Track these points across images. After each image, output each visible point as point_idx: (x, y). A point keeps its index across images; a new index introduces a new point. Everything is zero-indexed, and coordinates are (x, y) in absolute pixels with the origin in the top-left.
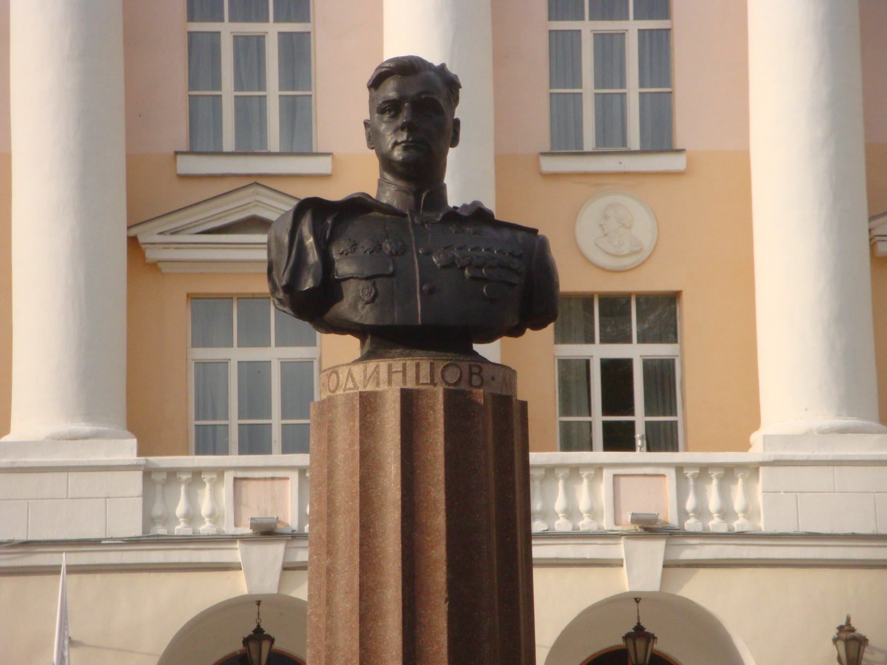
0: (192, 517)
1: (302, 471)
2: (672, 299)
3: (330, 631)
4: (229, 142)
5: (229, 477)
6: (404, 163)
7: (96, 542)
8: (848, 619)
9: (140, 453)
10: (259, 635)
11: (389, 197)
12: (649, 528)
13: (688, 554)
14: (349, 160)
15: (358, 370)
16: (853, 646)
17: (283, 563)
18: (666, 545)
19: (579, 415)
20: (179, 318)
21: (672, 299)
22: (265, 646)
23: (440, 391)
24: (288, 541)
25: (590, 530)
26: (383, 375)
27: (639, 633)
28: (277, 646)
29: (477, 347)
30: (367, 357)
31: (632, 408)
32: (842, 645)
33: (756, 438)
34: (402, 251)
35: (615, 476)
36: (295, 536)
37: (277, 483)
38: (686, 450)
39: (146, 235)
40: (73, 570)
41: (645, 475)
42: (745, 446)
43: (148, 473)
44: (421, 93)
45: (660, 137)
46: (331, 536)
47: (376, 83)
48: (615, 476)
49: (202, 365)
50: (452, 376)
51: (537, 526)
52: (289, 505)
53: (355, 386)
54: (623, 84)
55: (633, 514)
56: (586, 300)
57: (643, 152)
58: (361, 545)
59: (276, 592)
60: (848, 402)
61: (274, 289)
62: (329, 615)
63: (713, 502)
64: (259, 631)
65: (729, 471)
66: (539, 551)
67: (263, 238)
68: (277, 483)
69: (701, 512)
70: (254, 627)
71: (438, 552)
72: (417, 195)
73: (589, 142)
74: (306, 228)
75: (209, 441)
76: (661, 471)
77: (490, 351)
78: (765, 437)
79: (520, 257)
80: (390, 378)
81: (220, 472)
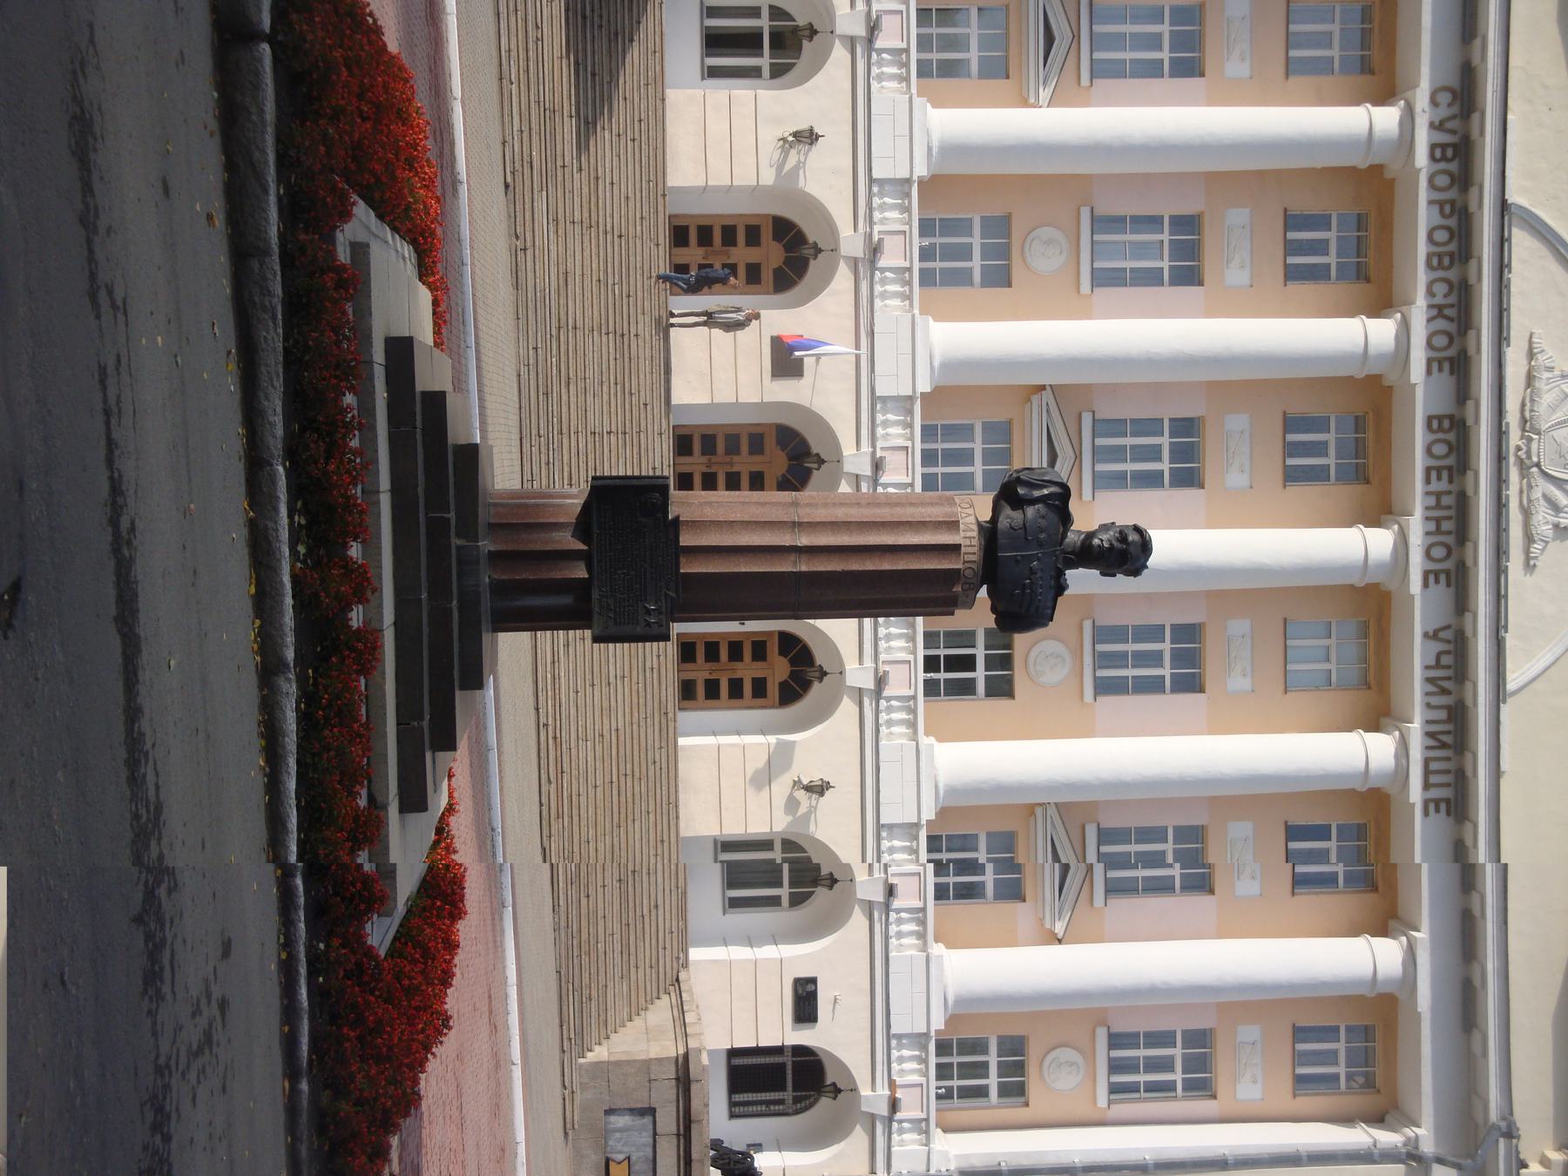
0: (886, 424)
1: (912, 485)
3: (826, 505)
4: (1100, 441)
5: (909, 444)
6: (1091, 545)
10: (821, 462)
11: (1072, 537)
12: (881, 681)
13: (866, 701)
14: (1094, 513)
15: (972, 519)
20: (999, 416)
25: (872, 651)
27: (823, 674)
30: (979, 525)
31: (949, 673)
33: (932, 740)
34: (1040, 545)
36: (875, 481)
39: (1047, 396)
40: (858, 357)
41: (501, 789)
42: (927, 734)
43: (911, 399)
45: (1105, 687)
46: (878, 505)
47: (1137, 529)
49: (971, 428)
51: (881, 620)
56: (1009, 646)
57: (1095, 678)
60: (952, 791)
61: (1018, 471)
64: (823, 462)
65: (913, 725)
66: (867, 622)
67: (1045, 465)
69: (890, 709)
71: (886, 565)
72: (1072, 553)
73: (1100, 648)
74: (1053, 489)
75: (928, 432)
77: (983, 592)
80: (968, 538)
81: (912, 438)
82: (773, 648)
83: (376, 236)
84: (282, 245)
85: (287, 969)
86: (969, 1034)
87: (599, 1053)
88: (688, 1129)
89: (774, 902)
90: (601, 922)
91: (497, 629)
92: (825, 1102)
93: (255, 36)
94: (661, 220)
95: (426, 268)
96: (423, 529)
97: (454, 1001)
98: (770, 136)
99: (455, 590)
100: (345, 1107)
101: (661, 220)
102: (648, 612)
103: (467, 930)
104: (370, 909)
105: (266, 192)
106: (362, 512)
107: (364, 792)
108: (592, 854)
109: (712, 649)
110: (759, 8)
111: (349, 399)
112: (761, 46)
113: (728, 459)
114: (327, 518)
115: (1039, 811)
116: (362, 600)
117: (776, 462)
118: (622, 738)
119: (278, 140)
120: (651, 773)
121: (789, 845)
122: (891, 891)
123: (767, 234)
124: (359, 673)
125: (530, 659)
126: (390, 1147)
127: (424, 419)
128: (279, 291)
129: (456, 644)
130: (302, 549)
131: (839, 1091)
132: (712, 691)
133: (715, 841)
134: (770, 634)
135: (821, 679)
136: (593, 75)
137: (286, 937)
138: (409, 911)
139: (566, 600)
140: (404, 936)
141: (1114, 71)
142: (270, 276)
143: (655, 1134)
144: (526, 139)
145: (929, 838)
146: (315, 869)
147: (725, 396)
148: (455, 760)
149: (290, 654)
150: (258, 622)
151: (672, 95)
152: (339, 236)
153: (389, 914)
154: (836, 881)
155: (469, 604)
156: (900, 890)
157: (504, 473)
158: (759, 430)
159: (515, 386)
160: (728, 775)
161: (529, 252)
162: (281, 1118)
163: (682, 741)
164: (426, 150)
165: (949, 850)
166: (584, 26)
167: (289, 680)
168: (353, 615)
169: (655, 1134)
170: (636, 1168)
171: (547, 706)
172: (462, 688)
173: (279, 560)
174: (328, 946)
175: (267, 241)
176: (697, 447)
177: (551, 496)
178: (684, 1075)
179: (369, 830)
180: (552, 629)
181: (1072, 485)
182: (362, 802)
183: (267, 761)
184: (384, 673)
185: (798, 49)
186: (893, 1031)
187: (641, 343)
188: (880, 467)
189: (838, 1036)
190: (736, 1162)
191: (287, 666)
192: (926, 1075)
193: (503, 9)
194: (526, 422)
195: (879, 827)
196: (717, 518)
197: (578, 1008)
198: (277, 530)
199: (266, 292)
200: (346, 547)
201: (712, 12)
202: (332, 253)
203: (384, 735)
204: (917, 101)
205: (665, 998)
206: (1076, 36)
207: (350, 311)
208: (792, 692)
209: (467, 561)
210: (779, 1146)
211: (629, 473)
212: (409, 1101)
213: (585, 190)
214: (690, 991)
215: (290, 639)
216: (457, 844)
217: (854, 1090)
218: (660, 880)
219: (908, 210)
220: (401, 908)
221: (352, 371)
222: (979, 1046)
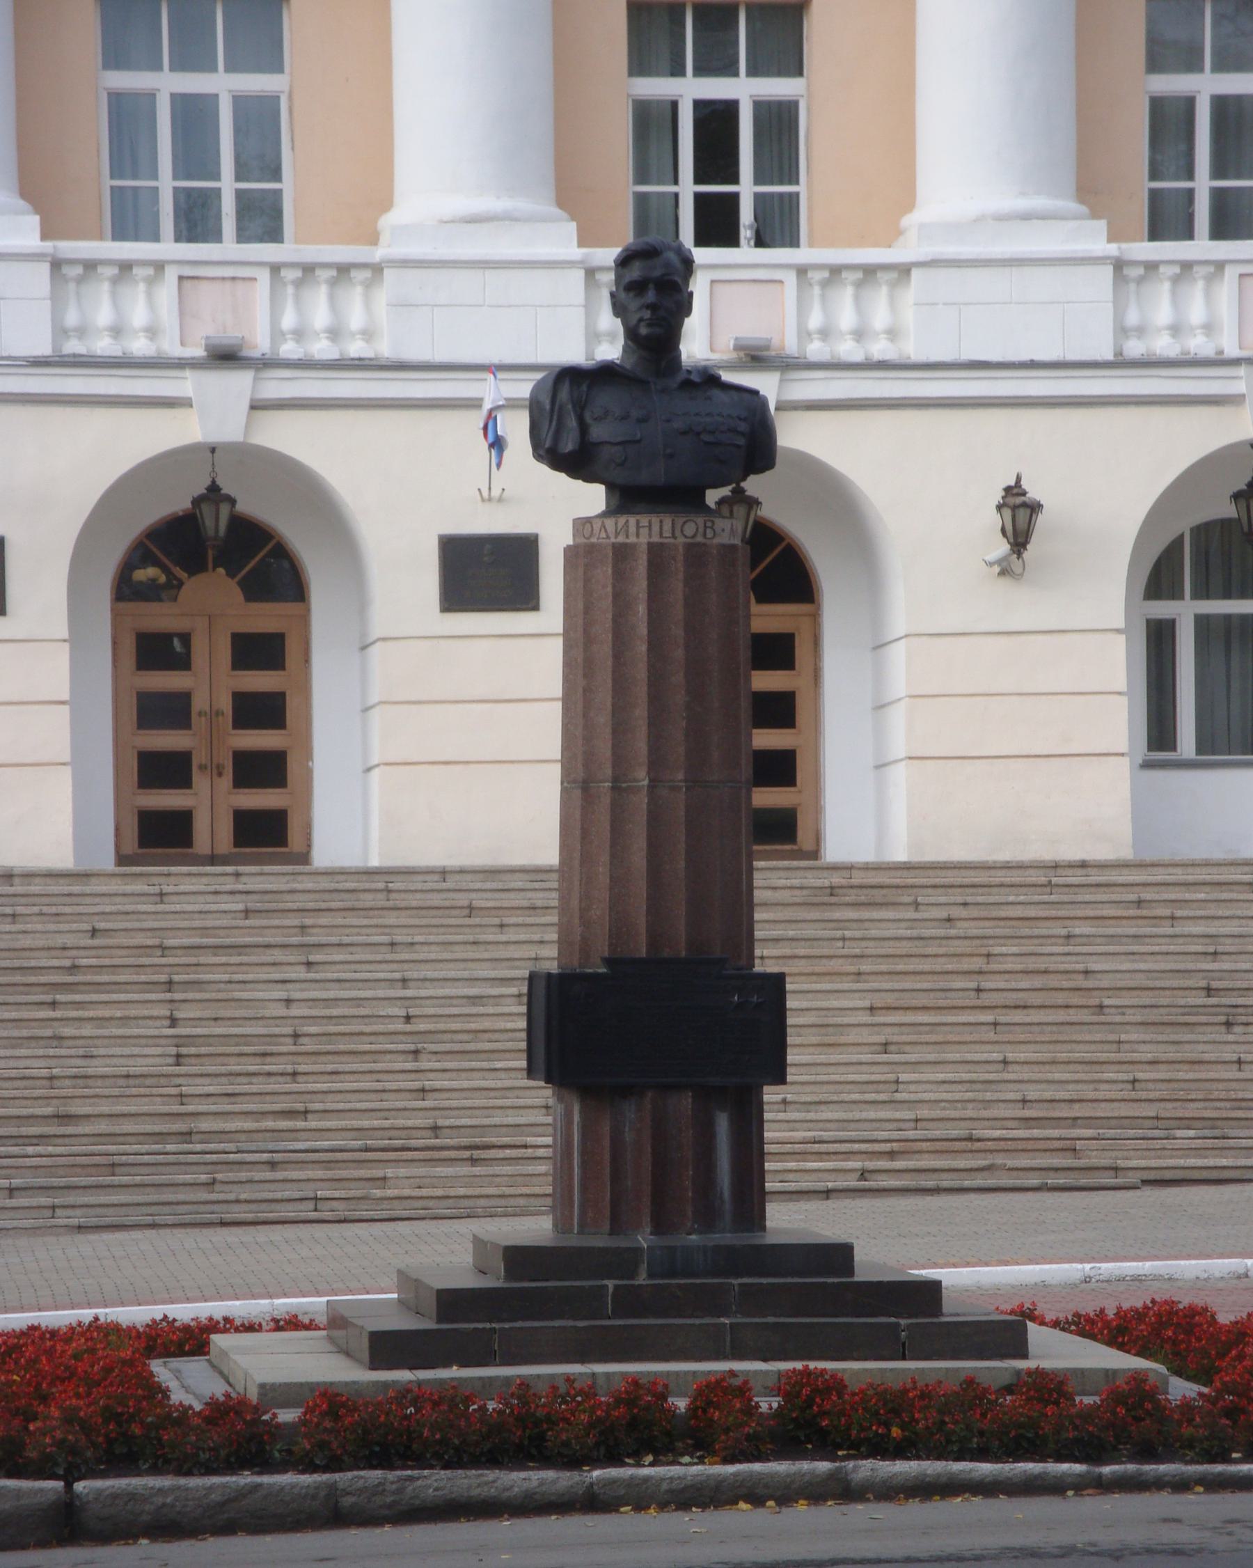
5: (171, 274)
6: (647, 337)
8: (1019, 479)
9: (45, 236)
15: (610, 523)
16: (1023, 514)
17: (252, 400)
18: (781, 381)
19: (659, 183)
22: (225, 511)
24: (258, 370)
26: (632, 529)
32: (1007, 513)
35: (713, 282)
37: (240, 285)
38: (811, 245)
42: (892, 234)
43: (57, 265)
44: (663, 275)
48: (713, 282)
50: (690, 529)
53: (608, 537)
55: (737, 339)
58: (614, 672)
59: (241, 439)
64: (214, 488)
65: (870, 272)
68: (240, 286)
70: (208, 482)
74: (564, 394)
76: (777, 275)
78: (922, 226)
79: (745, 420)
81: (159, 266)
91: (764, 1228)
108: (1161, 1073)
117: (212, 606)
118: (890, 999)
121: (1160, 579)
127: (462, 1320)
128: (377, 1474)
129: (789, 1280)
133: (1147, 765)
139: (723, 1124)
142: (361, 1483)
145: (1156, 233)
146: (1092, 1451)
147: (52, 733)
149: (824, 1466)
158: (129, 644)
159: (108, 1237)
163: (900, 855)
167: (855, 1468)
172: (851, 1272)
173: (708, 1476)
175: (318, 1487)
176: (167, 800)
179: (1049, 1388)
191: (838, 1470)
195: (1120, 363)
198: (671, 1479)
199: (379, 1489)
215: (805, 1466)
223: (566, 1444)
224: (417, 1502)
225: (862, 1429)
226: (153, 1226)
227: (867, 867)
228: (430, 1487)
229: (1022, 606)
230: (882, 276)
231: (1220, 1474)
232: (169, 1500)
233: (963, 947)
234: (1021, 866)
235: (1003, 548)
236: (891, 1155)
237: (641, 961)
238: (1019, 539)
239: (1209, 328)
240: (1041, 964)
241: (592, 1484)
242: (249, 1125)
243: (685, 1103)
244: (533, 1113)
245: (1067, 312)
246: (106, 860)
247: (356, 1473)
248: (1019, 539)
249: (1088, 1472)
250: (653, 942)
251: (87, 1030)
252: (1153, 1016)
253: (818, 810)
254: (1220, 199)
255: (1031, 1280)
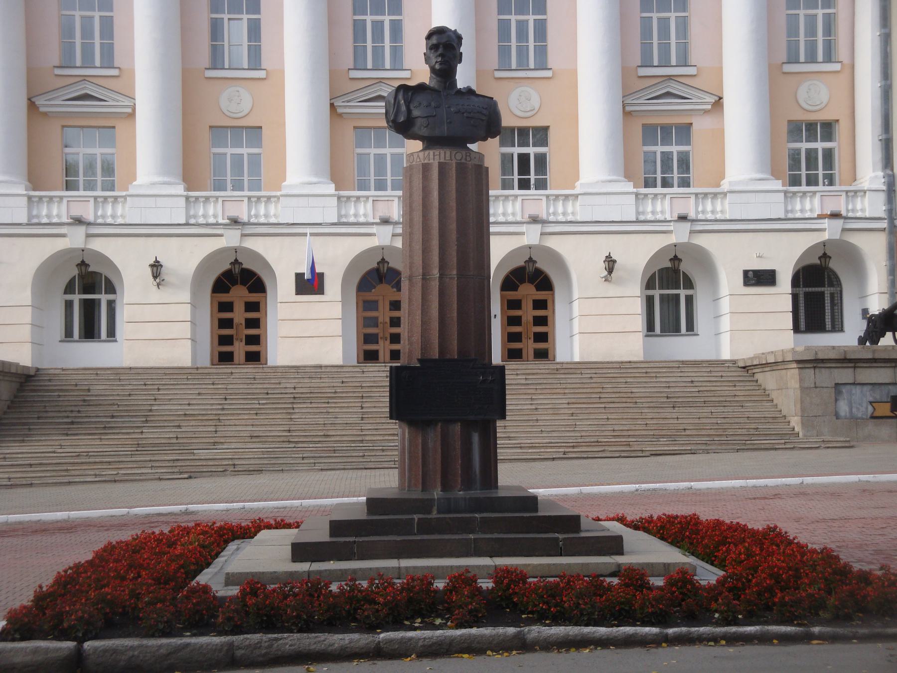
1: (399, 197)
2: (545, 129)
5: (371, 199)
7: (320, 224)
10: (383, 261)
12: (535, 220)
14: (418, 69)
15: (421, 154)
16: (611, 263)
21: (545, 129)
22: (386, 265)
23: (454, 162)
25: (512, 226)
26: (431, 156)
27: (531, 260)
28: (390, 265)
29: (468, 145)
31: (529, 173)
33: (578, 184)
36: (396, 223)
39: (337, 103)
40: (312, 234)
42: (573, 188)
43: (339, 198)
45: (542, 65)
47: (429, 37)
50: (459, 156)
51: (492, 219)
52: (395, 211)
54: (527, 42)
56: (512, 129)
61: (388, 122)
62: (411, 251)
63: (560, 209)
64: (383, 259)
65: (567, 197)
74: (400, 96)
75: (363, 186)
77: (473, 147)
81: (367, 197)
82: (512, 295)
83: (222, 568)
84: (226, 633)
85: (732, 640)
86: (786, 162)
87: (796, 422)
88: (850, 361)
89: (690, 300)
90: (704, 421)
91: (496, 487)
92: (833, 265)
93: (78, 657)
94: (214, 371)
95: (246, 531)
96: (426, 537)
97: (756, 521)
98: (156, 295)
99: (471, 515)
100: (832, 601)
101: (214, 371)
102: (484, 381)
103: (706, 514)
104: (691, 582)
105: (188, 645)
106: (412, 578)
107: (608, 580)
108: (655, 422)
109: (513, 337)
110: (66, 301)
111: (334, 587)
112: (93, 300)
113: (380, 326)
114: (417, 603)
115: (628, 109)
116: (474, 579)
117: (239, 295)
118: (573, 401)
119: (153, 636)
120: (599, 380)
121: (649, 284)
122: (683, 218)
123: (224, 298)
124: (525, 582)
125: (519, 464)
126: (860, 570)
127: (348, 537)
130: (438, 621)
131: (825, 254)
132: (542, 337)
133: (647, 336)
134: (502, 297)
135: (535, 262)
136: (113, 417)
137: (709, 640)
138: (693, 554)
139: (476, 438)
140: (710, 558)
141: (108, 53)
142: (247, 642)
143: (854, 384)
144: (157, 464)
146: (661, 620)
147: (337, 327)
148: (587, 517)
149: (511, 630)
150: (489, 652)
151: (127, 363)
152: (221, 594)
153: (695, 568)
154: (676, 257)
155: (479, 505)
156: (683, 212)
157: (387, 481)
158: (361, 304)
160: (597, 324)
161: (236, 462)
162: (838, 646)
163: (577, 359)
164: (162, 533)
165: (655, 173)
166: (78, 423)
168: (484, 586)
169: (854, 384)
170: (878, 397)
171: (551, 452)
172: (536, 510)
174: (716, 611)
175: (218, 648)
177: (403, 448)
178: (814, 363)
179: (635, 578)
180: (496, 448)
181: (397, 84)
182: (615, 581)
183: (586, 647)
184: (525, 565)
185: (94, 273)
186: (783, 216)
187: (300, 385)
188: (379, 220)
189: (785, 256)
190: (875, 326)
191: (519, 632)
192: (815, 193)
193: (66, 480)
194: (354, 466)
195: (638, 221)
196: (415, 337)
197: (762, 437)
200: (436, 591)
201: (69, 333)
202: (231, 598)
203: (569, 565)
204: (132, 191)
205: (757, 376)
206: (85, 78)
207: (273, 586)
208: (544, 283)
209: (448, 506)
210: (863, 297)
211: (388, 394)
212: (828, 557)
213: (193, 423)
214: (752, 359)
215: (501, 630)
216: (645, 515)
217: (824, 244)
218: (673, 379)
219: (207, 199)
220: (691, 560)
221: (314, 587)
222: (795, 157)
223: (368, 617)
224: (280, 653)
225: (535, 605)
226: (344, 469)
227: (567, 363)
228: (287, 644)
229: (612, 290)
230: (570, 198)
231: (735, 633)
232: (136, 653)
233: (594, 385)
234: (612, 363)
235: (606, 273)
236: (573, 447)
237: (435, 360)
238: (610, 270)
239: (662, 212)
240: (618, 390)
241: (379, 642)
242: (381, 438)
243: (457, 428)
244: (392, 435)
245: (623, 207)
246: (207, 363)
247: (245, 636)
248: (610, 270)
249: (661, 633)
250: (441, 352)
251: (337, 410)
252: (652, 405)
253: (554, 349)
254: (663, 179)
255: (618, 490)
